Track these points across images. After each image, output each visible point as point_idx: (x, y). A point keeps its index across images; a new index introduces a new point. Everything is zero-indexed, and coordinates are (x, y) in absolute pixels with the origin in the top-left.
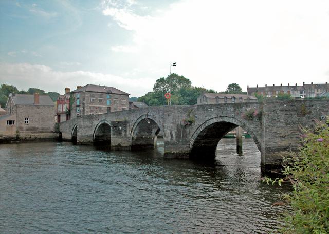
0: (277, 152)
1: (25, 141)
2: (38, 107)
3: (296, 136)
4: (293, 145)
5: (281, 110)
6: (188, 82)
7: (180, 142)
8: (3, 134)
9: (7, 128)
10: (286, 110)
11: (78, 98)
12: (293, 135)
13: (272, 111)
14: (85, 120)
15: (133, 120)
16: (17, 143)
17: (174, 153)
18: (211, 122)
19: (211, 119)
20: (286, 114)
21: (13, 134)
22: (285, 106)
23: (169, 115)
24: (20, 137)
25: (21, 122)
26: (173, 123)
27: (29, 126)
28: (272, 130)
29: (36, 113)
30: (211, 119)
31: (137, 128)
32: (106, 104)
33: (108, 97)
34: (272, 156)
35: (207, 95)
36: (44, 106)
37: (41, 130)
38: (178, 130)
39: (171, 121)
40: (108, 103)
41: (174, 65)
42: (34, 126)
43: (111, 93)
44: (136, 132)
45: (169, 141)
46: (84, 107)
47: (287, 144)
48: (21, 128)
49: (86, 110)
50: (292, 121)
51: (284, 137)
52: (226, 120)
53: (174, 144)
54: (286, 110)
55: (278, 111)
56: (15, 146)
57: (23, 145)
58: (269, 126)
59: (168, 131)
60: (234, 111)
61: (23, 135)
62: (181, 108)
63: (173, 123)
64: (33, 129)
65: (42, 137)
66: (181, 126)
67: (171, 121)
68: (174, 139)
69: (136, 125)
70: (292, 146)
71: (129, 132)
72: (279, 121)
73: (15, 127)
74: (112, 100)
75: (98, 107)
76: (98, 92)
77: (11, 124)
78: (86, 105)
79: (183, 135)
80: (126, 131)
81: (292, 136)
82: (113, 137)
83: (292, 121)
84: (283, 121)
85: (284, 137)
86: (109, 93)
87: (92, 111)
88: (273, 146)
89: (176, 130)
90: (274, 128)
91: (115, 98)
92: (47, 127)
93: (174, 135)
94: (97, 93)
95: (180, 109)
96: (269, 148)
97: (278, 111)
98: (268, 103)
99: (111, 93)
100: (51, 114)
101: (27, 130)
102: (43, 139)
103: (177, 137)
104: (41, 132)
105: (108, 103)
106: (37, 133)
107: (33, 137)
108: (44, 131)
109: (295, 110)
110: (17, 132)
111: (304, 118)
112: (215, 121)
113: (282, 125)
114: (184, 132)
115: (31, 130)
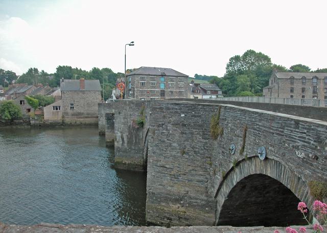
0: (164, 204)
1: (71, 126)
2: (83, 92)
3: (197, 178)
4: (192, 195)
5: (175, 124)
6: (267, 59)
7: (132, 149)
8: (50, 119)
9: (53, 113)
10: (184, 125)
11: (130, 82)
12: (192, 175)
13: (159, 126)
14: (105, 108)
16: (63, 129)
17: (125, 164)
20: (182, 133)
21: (59, 119)
22: (183, 115)
23: (119, 113)
24: (65, 122)
25: (66, 107)
26: (124, 124)
27: (75, 111)
28: (157, 161)
29: (81, 98)
32: (159, 87)
33: (162, 79)
34: (157, 209)
35: (278, 75)
36: (89, 91)
37: (86, 116)
38: (130, 133)
39: (122, 121)
40: (162, 86)
41: (132, 44)
42: (79, 111)
43: (165, 76)
45: (120, 146)
46: (134, 91)
47: (182, 191)
48: (67, 114)
49: (136, 94)
50: (193, 148)
51: (175, 177)
53: (125, 151)
54: (184, 125)
55: (170, 127)
56: (60, 132)
57: (70, 132)
58: (154, 153)
59: (119, 134)
61: (68, 120)
63: (124, 124)
64: (79, 115)
65: (87, 122)
66: (134, 128)
67: (122, 121)
68: (126, 145)
70: (191, 198)
72: (170, 145)
73: (61, 112)
74: (167, 82)
75: (150, 91)
76: (149, 75)
77: (57, 109)
78: (135, 89)
79: (136, 140)
81: (191, 177)
82: (107, 132)
83: (193, 148)
84: (175, 145)
85: (175, 177)
86: (162, 76)
87: (142, 95)
88: (158, 191)
89: (127, 134)
90: (162, 158)
91: (170, 81)
92: (92, 112)
93: (125, 139)
94: (148, 76)
95: (132, 105)
96: (153, 193)
97: (170, 127)
98: (154, 109)
99: (165, 76)
100: (97, 99)
101: (73, 115)
102: (88, 124)
103: (128, 142)
104: (86, 117)
105: (162, 86)
106: (82, 118)
107: (78, 123)
108: (90, 116)
109: (200, 126)
110: (63, 117)
111: (216, 142)
113: (174, 153)
114: (137, 136)
115: (77, 115)
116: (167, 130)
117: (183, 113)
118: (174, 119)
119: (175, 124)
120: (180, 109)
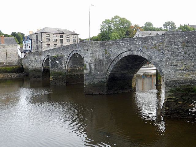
13: (172, 44)
15: (66, 54)
18: (123, 55)
19: (123, 53)
30: (123, 53)
31: (70, 62)
38: (96, 62)
44: (69, 65)
52: (135, 53)
55: (179, 44)
60: (141, 45)
62: (98, 43)
69: (69, 59)
71: (64, 65)
80: (62, 64)
85: (185, 70)
90: (175, 61)
93: (92, 67)
97: (179, 44)
112: (126, 54)
116: (177, 45)
117: (187, 36)
118: (182, 39)
119: (182, 42)
120: (185, 34)
